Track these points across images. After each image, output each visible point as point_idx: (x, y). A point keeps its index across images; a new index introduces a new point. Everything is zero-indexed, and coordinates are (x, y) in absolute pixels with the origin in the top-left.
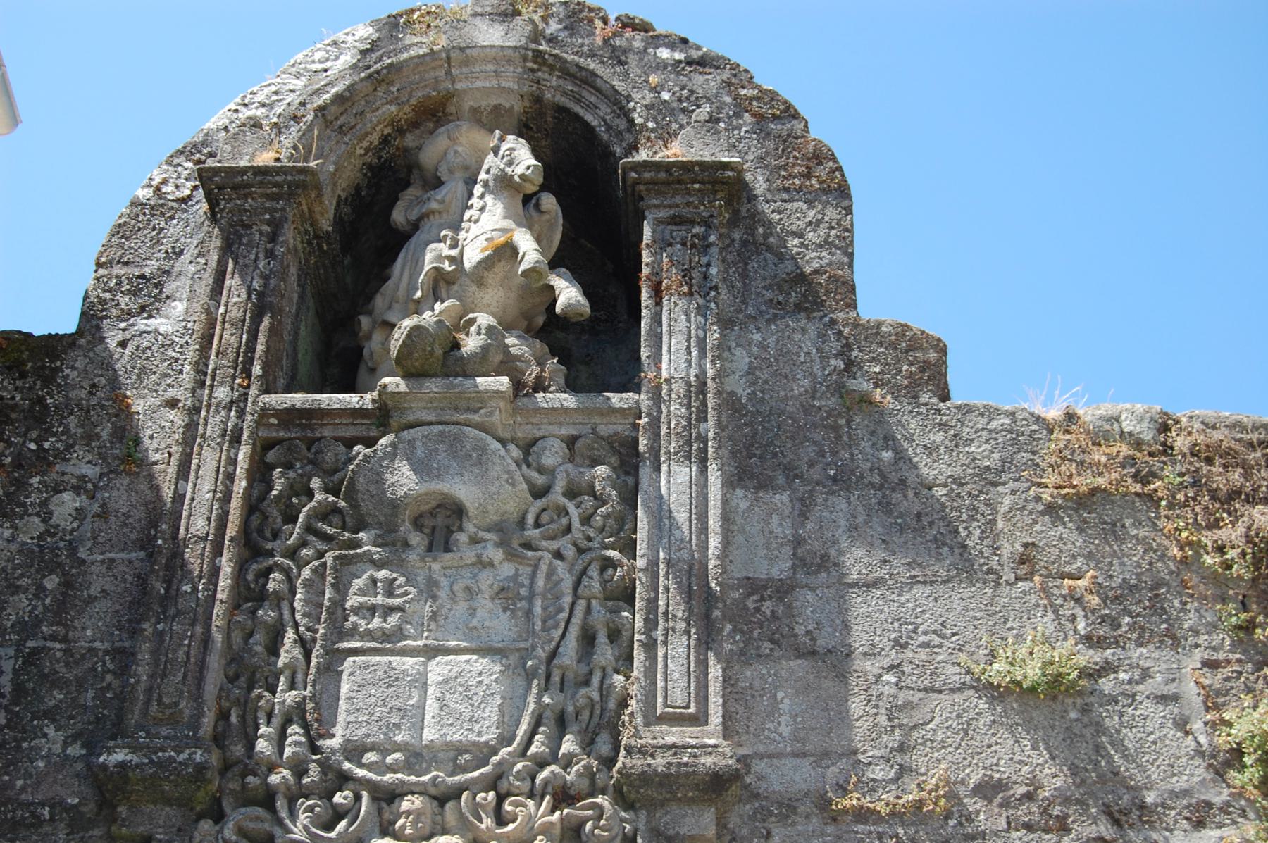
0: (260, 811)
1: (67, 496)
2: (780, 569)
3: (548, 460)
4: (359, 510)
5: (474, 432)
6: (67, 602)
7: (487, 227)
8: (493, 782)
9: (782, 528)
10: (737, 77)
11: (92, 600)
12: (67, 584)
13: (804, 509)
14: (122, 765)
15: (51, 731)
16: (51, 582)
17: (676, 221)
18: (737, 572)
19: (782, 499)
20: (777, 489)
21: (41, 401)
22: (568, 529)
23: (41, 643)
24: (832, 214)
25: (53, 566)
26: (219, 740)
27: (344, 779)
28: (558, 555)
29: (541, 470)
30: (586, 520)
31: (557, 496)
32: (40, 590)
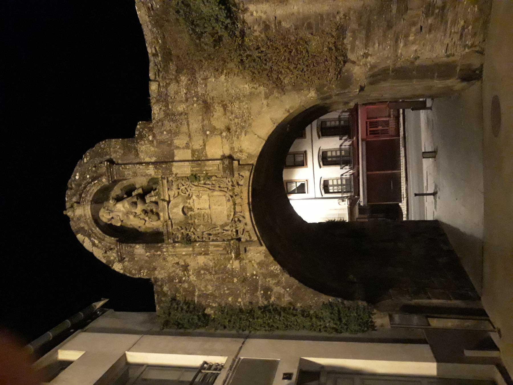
2: (189, 151)
5: (169, 207)
11: (205, 265)
12: (203, 269)
13: (178, 148)
32: (204, 274)
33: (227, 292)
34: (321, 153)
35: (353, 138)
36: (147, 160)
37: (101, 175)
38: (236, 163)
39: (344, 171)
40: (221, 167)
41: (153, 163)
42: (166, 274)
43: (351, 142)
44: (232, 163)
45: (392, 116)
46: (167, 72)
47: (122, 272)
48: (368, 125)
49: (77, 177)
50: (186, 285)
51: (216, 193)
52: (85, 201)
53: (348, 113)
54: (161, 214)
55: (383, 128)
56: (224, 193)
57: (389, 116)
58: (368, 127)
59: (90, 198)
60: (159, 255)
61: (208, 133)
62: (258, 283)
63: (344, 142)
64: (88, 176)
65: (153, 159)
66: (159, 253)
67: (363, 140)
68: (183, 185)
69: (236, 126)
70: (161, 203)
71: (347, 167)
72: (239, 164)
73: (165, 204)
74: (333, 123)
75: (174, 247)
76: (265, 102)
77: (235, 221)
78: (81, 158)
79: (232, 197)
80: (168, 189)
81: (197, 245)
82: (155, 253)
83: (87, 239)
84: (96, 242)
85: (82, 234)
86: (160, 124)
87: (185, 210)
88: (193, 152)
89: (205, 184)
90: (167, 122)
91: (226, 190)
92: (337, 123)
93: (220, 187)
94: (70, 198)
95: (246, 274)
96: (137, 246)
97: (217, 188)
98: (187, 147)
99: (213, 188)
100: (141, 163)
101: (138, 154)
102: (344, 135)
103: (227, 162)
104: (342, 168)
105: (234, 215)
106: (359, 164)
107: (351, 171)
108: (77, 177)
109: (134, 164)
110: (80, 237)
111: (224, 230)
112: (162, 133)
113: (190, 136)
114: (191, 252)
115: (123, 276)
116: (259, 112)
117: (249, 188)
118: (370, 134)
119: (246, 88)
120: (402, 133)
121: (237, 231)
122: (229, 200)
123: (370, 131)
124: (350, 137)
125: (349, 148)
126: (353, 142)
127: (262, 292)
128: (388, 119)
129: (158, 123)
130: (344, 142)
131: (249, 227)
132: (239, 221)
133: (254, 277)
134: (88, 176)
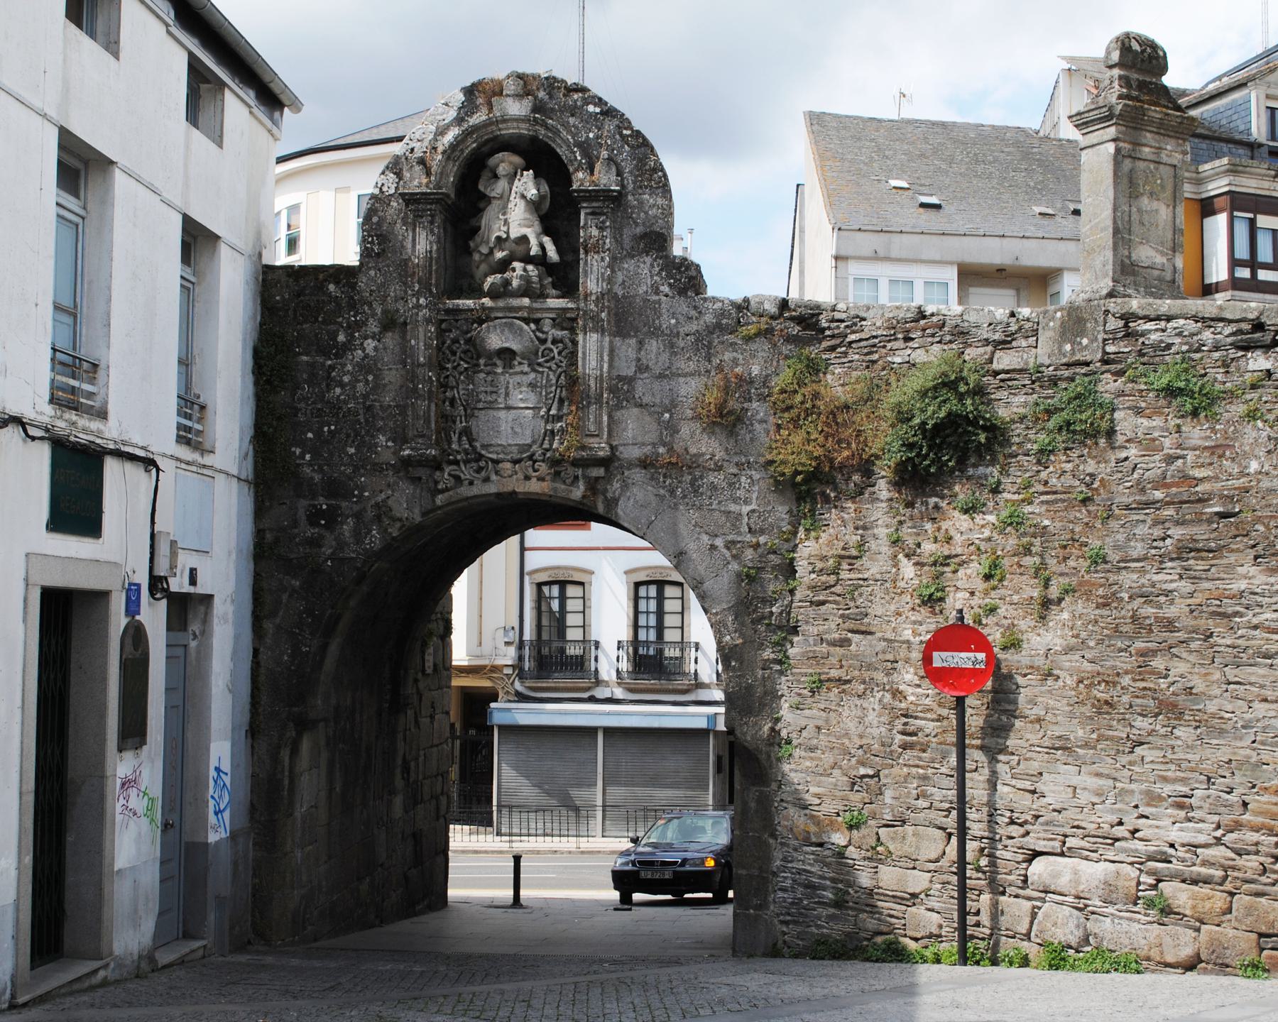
0: (455, 467)
1: (370, 341)
2: (630, 372)
3: (545, 329)
4: (475, 351)
5: (518, 322)
6: (378, 387)
7: (514, 213)
8: (531, 458)
9: (632, 354)
10: (624, 122)
11: (385, 385)
12: (376, 377)
13: (641, 343)
14: (409, 456)
16: (370, 378)
17: (592, 214)
18: (615, 373)
19: (633, 341)
20: (630, 336)
21: (352, 298)
22: (553, 358)
24: (660, 201)
25: (369, 372)
26: (438, 442)
27: (481, 456)
28: (550, 368)
29: (543, 332)
30: (560, 353)
31: (549, 345)
50: (341, 338)
76: (719, 542)
80: (553, 319)
98: (642, 368)
105: (494, 461)
111: (460, 434)
113: (661, 376)
121: (456, 463)
131: (465, 491)
132: (479, 470)
134: (591, 135)
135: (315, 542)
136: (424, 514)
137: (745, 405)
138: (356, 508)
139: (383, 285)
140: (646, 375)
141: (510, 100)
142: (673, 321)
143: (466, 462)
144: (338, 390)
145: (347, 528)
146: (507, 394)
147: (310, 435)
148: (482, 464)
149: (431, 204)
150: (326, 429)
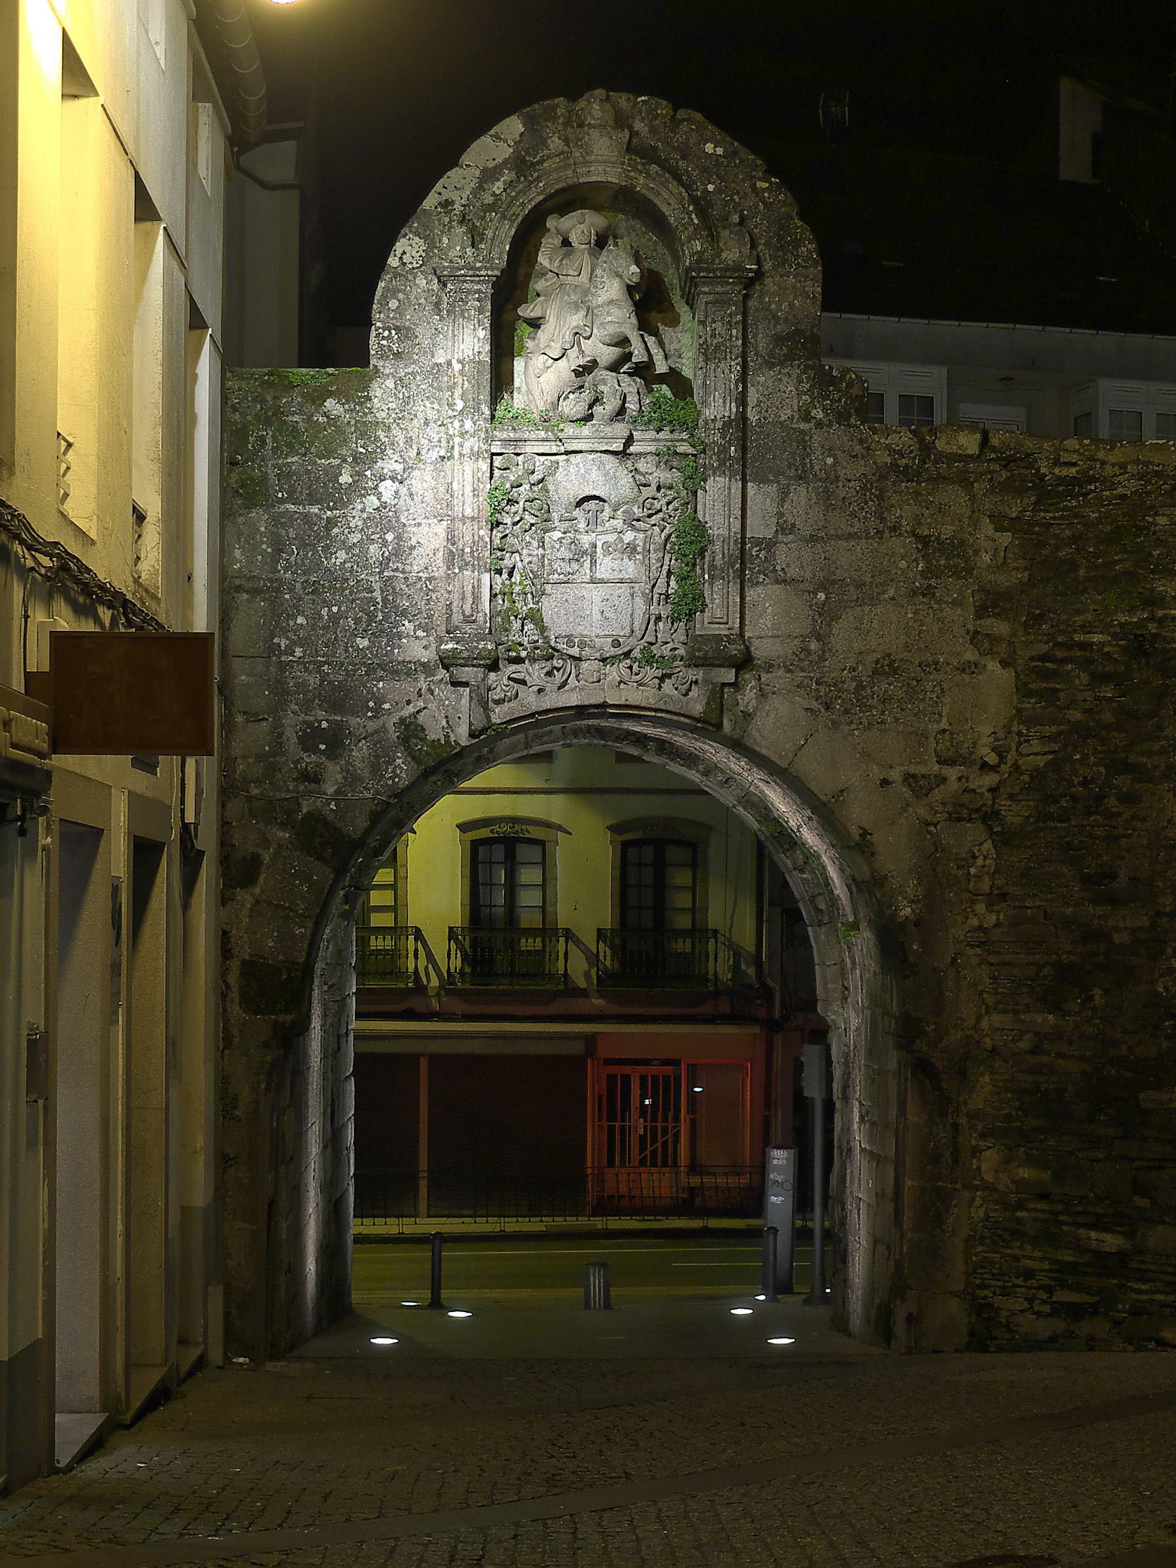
1: (388, 482)
11: (413, 548)
12: (399, 537)
15: (406, 623)
20: (768, 482)
23: (392, 573)
32: (385, 543)
33: (324, 612)
34: (536, 833)
35: (601, 994)
36: (753, 396)
37: (713, 238)
38: (729, 676)
39: (439, 944)
40: (722, 630)
41: (743, 417)
42: (384, 415)
43: (582, 984)
44: (731, 666)
45: (695, 1181)
46: (1005, 487)
47: (393, 262)
48: (656, 1069)
49: (709, 148)
50: (345, 478)
51: (640, 602)
52: (635, 169)
53: (726, 976)
54: (586, 430)
55: (635, 1140)
56: (639, 634)
57: (694, 1168)
58: (643, 1069)
59: (641, 184)
60: (451, 405)
61: (821, 596)
62: (355, 713)
63: (586, 951)
64: (711, 187)
65: (752, 416)
66: (460, 405)
67: (590, 1040)
68: (668, 504)
69: (835, 685)
70: (621, 429)
71: (457, 963)
72: (724, 685)
73: (618, 446)
74: (683, 900)
75: (476, 455)
76: (895, 775)
77: (552, 657)
78: (770, 172)
79: (627, 655)
81: (482, 532)
82: (458, 392)
83: (504, 152)
84: (498, 187)
85: (522, 135)
86: (858, 448)
87: (592, 505)
88: (768, 545)
89: (669, 573)
90: (862, 470)
91: (649, 637)
92: (683, 922)
93: (659, 618)
94: (647, 113)
95: (381, 679)
96: (482, 334)
97: (654, 609)
98: (785, 528)
99: (656, 596)
100: (743, 378)
101: (771, 366)
102: (620, 951)
103: (734, 650)
104: (452, 934)
105: (571, 657)
106: (467, 1018)
107: (435, 982)
108: (709, 148)
109: (744, 355)
110: (513, 126)
112: (830, 451)
113: (813, 539)
114: (458, 509)
115: (379, 266)
116: (869, 756)
117: (650, 709)
118: (611, 1078)
119: (939, 722)
120: (615, 1223)
121: (518, 660)
122: (616, 643)
123: (626, 1079)
124: (607, 981)
125: (551, 976)
126: (584, 993)
127: (324, 725)
128: (683, 1159)
129: (861, 441)
130: (586, 951)
133: (371, 704)
134: (711, 187)
135: (313, 778)
136: (472, 735)
137: (933, 582)
138: (371, 726)
139: (958, 972)
140: (791, 537)
141: (595, 133)
142: (830, 461)
143: (533, 660)
144: (342, 555)
145: (360, 753)
146: (593, 563)
147: (300, 620)
148: (557, 663)
149: (479, 282)
150: (324, 612)
